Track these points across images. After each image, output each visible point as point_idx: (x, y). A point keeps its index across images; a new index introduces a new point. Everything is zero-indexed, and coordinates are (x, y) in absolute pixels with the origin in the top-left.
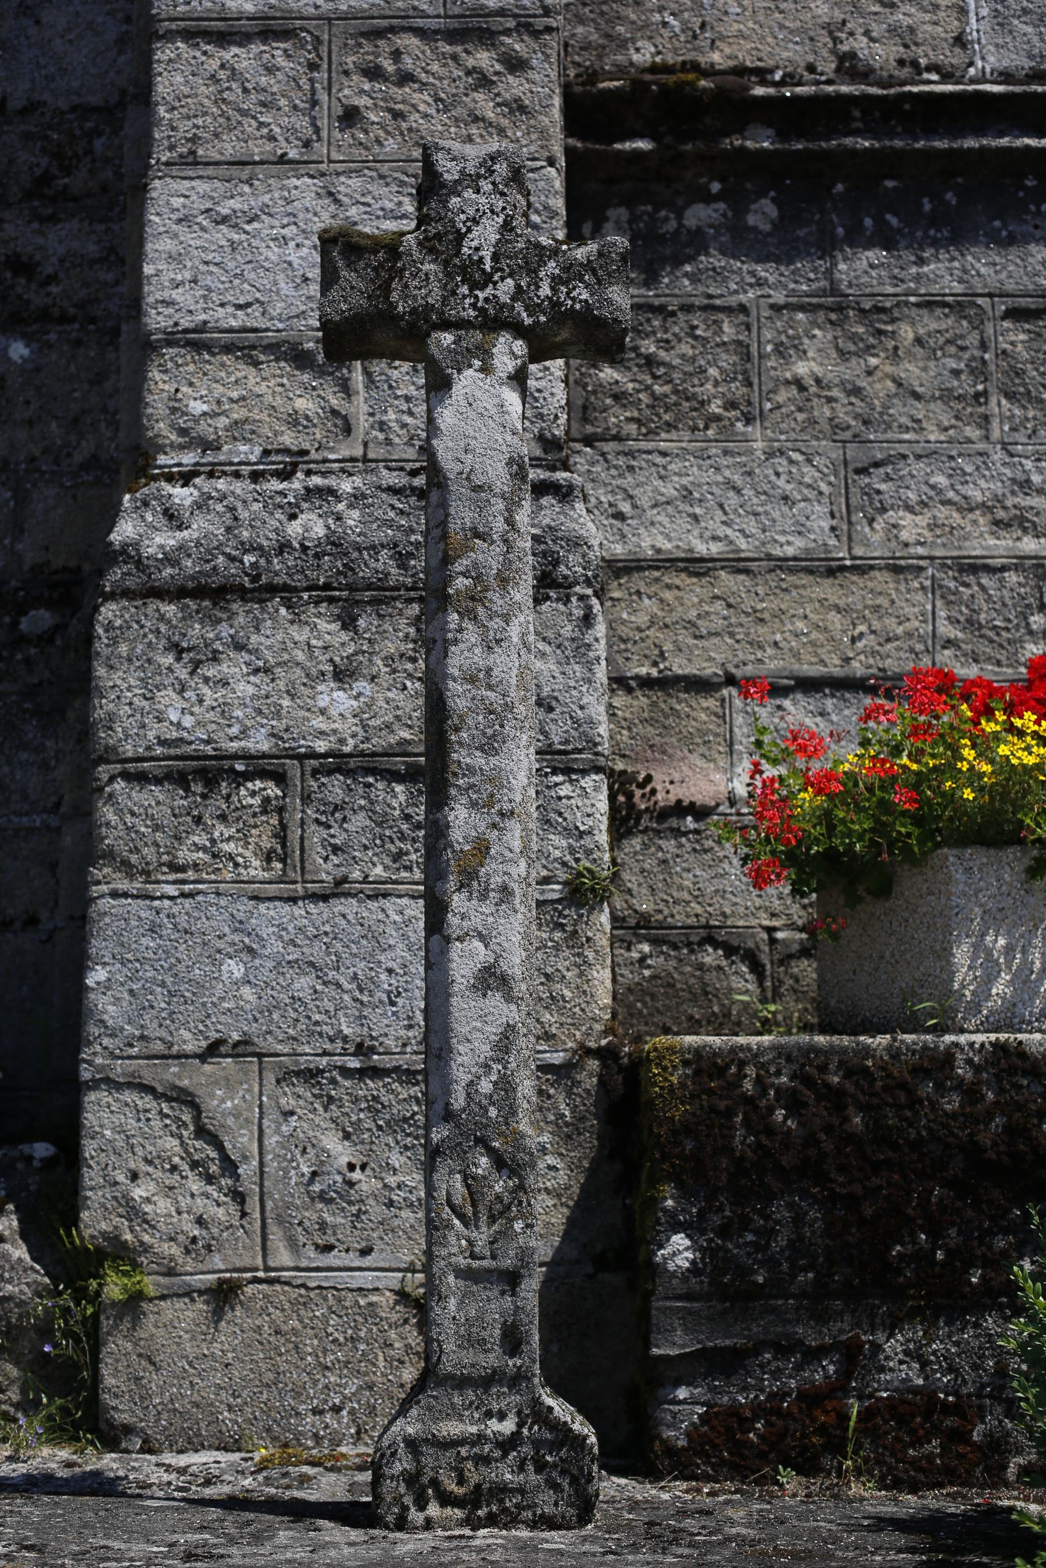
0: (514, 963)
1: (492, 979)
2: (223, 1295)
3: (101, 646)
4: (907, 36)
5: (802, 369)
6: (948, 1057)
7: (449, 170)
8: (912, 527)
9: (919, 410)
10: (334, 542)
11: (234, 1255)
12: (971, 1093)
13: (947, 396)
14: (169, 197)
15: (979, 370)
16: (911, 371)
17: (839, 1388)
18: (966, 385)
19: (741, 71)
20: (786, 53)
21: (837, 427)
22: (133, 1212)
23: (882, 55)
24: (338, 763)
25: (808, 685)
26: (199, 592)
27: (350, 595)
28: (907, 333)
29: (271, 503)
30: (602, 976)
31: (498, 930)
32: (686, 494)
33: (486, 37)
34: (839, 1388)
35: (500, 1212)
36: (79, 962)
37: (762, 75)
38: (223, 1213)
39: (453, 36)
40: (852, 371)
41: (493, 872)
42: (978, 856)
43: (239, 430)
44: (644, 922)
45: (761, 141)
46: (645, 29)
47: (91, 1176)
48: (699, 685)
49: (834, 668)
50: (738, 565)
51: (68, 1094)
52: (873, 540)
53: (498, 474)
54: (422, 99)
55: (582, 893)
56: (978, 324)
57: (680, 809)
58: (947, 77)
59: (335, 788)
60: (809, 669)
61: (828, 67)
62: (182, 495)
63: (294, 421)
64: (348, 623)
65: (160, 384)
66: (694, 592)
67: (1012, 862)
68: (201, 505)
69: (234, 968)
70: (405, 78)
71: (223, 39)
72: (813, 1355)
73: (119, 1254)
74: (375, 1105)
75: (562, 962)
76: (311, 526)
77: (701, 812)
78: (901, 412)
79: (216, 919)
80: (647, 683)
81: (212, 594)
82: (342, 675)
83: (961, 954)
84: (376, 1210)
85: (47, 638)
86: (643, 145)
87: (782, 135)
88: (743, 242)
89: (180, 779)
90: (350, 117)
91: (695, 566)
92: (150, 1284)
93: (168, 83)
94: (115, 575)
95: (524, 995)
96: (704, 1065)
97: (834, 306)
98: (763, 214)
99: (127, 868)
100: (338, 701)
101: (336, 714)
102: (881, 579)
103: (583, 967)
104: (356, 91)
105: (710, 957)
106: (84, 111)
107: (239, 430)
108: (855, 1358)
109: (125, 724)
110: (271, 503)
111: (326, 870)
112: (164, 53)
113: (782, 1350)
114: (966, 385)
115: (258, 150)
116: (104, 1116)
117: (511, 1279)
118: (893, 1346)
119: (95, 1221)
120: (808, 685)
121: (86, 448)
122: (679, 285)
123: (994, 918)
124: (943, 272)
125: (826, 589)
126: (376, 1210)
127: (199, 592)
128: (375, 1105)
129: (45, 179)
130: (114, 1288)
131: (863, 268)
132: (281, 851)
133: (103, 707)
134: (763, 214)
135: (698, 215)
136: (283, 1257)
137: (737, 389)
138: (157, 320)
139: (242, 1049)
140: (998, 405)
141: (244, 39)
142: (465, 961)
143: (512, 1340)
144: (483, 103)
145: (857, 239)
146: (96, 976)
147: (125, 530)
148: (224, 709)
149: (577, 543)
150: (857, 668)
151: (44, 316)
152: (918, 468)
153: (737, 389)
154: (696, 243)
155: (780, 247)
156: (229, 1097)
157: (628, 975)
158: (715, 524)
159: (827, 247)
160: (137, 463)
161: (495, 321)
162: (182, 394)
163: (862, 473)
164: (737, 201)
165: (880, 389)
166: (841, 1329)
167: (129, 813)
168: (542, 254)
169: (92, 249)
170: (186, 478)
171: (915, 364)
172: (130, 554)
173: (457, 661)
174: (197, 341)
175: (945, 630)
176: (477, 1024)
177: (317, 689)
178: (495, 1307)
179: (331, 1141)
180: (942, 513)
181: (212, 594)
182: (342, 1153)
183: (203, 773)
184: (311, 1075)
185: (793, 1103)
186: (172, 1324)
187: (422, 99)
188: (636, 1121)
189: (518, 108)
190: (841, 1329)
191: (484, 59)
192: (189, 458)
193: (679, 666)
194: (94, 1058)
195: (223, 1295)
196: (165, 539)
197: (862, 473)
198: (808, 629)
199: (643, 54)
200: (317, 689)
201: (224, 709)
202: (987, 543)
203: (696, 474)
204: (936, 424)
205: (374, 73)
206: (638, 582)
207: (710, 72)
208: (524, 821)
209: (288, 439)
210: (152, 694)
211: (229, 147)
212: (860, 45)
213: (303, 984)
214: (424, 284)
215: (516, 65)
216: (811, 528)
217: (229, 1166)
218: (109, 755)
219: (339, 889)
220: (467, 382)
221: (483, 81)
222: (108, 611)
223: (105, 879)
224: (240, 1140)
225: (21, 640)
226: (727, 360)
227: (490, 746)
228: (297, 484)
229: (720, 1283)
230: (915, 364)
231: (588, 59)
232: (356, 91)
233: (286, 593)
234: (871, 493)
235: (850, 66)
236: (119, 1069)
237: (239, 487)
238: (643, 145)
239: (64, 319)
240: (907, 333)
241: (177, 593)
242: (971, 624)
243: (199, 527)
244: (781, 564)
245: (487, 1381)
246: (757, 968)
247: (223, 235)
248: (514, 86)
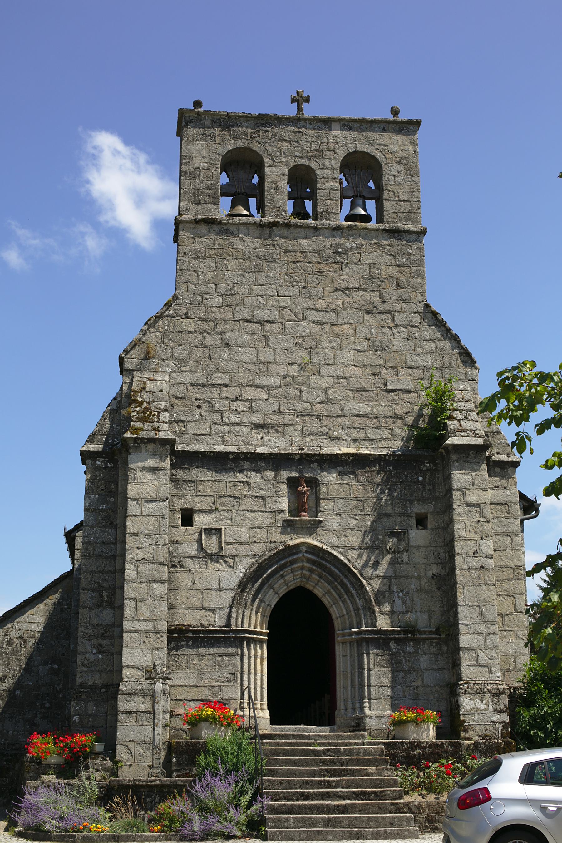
0: (160, 733)
1: (158, 734)
2: (130, 765)
3: (118, 700)
4: (208, 621)
5: (194, 662)
6: (200, 742)
7: (156, 664)
8: (206, 681)
9: (207, 667)
10: (142, 689)
11: (132, 761)
12: (202, 745)
13: (211, 666)
14: (125, 651)
15: (215, 663)
16: (207, 663)
17: (189, 773)
18: (213, 665)
19: (188, 625)
20: (194, 623)
21: (198, 669)
22: (121, 757)
23: (205, 623)
24: (143, 712)
25: (193, 700)
26: (128, 694)
27: (144, 695)
28: (207, 658)
29: (136, 684)
30: (168, 734)
31: (159, 730)
32: (180, 677)
33: (159, 633)
34: (189, 773)
35: (159, 753)
36: (116, 732)
37: (191, 626)
38: (130, 757)
39: (155, 633)
40: (200, 663)
41: (159, 725)
42: (205, 722)
43: (132, 676)
44: (174, 728)
45: (190, 635)
46: (177, 620)
47: (117, 754)
48: (181, 700)
49: (196, 698)
50: (186, 686)
51: (115, 745)
52: (201, 683)
53: (160, 692)
54: (152, 640)
55: (166, 726)
56: (215, 657)
57: (178, 715)
58: (213, 626)
59: (142, 715)
60: (193, 698)
61: (199, 625)
62: (126, 683)
63: (138, 676)
64: (144, 698)
65: (124, 671)
66: (181, 689)
67: (208, 723)
68: (128, 685)
69: (132, 733)
70: (150, 638)
71: (131, 633)
72: (187, 770)
73: (120, 761)
74: (145, 747)
75: (164, 733)
76: (140, 687)
77: (180, 715)
78: (205, 668)
79: (130, 728)
80: (175, 700)
81: (130, 694)
82: (143, 703)
83: (203, 732)
84: (145, 757)
85: (104, 692)
86: (176, 635)
87: (193, 634)
88: (188, 647)
89: (127, 714)
90: (144, 642)
91: (181, 686)
92: (123, 764)
93: (125, 637)
94: (120, 692)
95: (162, 736)
96: (177, 742)
97: (198, 655)
98: (190, 643)
99: (121, 723)
100: (143, 706)
101: (142, 707)
102: (202, 688)
103: (166, 733)
104: (145, 639)
105: (181, 732)
106: (108, 625)
107: (132, 676)
108: (191, 770)
109: (121, 708)
110: (136, 684)
111: (141, 723)
112: (124, 634)
113: (184, 769)
114: (213, 665)
115: (134, 645)
116: (118, 748)
117: (159, 759)
118: (194, 769)
119: (118, 758)
120: (193, 700)
121: (109, 669)
122: (180, 652)
123: (206, 729)
124: (211, 651)
125: (196, 689)
126: (145, 757)
127: (128, 694)
128: (145, 747)
129: (103, 634)
130: (119, 765)
131: (202, 650)
132: (137, 721)
133: (119, 706)
134: (190, 643)
135: (183, 643)
136: (136, 762)
137: (186, 665)
138: (124, 664)
139: (133, 741)
140: (217, 667)
141: (133, 633)
142: (156, 733)
143: (160, 764)
144: (158, 641)
145: (201, 647)
146: (118, 734)
147: (121, 687)
148: (131, 707)
149: (167, 690)
150: (199, 698)
151: (103, 652)
152: (207, 674)
153: (186, 665)
154: (182, 647)
155: (192, 647)
156: (131, 746)
157: (172, 734)
158: (183, 681)
159: (198, 647)
160: (121, 680)
161: (160, 678)
162: (126, 673)
163: (201, 675)
164: (187, 641)
165: (203, 665)
166: (189, 767)
167: (121, 717)
168: (164, 672)
169: (109, 643)
170: (127, 682)
171: (207, 662)
172: (121, 690)
173: (156, 708)
174: (128, 667)
175: (210, 694)
176: (157, 738)
177: (140, 704)
178: (158, 761)
179: (141, 750)
180: (210, 680)
181: (130, 694)
182: (142, 751)
183: (129, 713)
184: (139, 744)
185: (185, 746)
186: (125, 768)
187: (152, 640)
188: (171, 748)
189: (162, 641)
190: (189, 767)
191: (158, 636)
192: (127, 679)
193: (179, 698)
194: (117, 742)
195: (130, 765)
196: (125, 689)
197: (201, 675)
198: (194, 694)
199: (177, 623)
200: (140, 704)
201: (131, 707)
202: (215, 684)
203: (181, 675)
204: (209, 669)
205: (147, 637)
206: (174, 688)
207: (185, 625)
208: (162, 718)
209: (137, 677)
210: (123, 705)
211: (131, 645)
212: (203, 622)
213: (139, 734)
214: (154, 674)
215: (162, 636)
216: (194, 682)
217: (131, 753)
218: (119, 711)
219: (142, 725)
220: (157, 683)
221: (158, 638)
222: (119, 696)
223: (119, 724)
224: (132, 750)
225: (101, 693)
226: (185, 661)
227: (159, 715)
228: (138, 683)
229: (178, 763)
230: (207, 662)
231: (170, 623)
232: (145, 639)
233: (137, 694)
234: (201, 677)
235: (202, 625)
236: (120, 743)
237: (133, 683)
238: (176, 635)
239: (106, 652)
240: (207, 658)
241: (126, 694)
242: (212, 693)
243: (128, 687)
244: (191, 686)
245: (157, 767)
246: (186, 733)
247: (131, 655)
248: (162, 639)
